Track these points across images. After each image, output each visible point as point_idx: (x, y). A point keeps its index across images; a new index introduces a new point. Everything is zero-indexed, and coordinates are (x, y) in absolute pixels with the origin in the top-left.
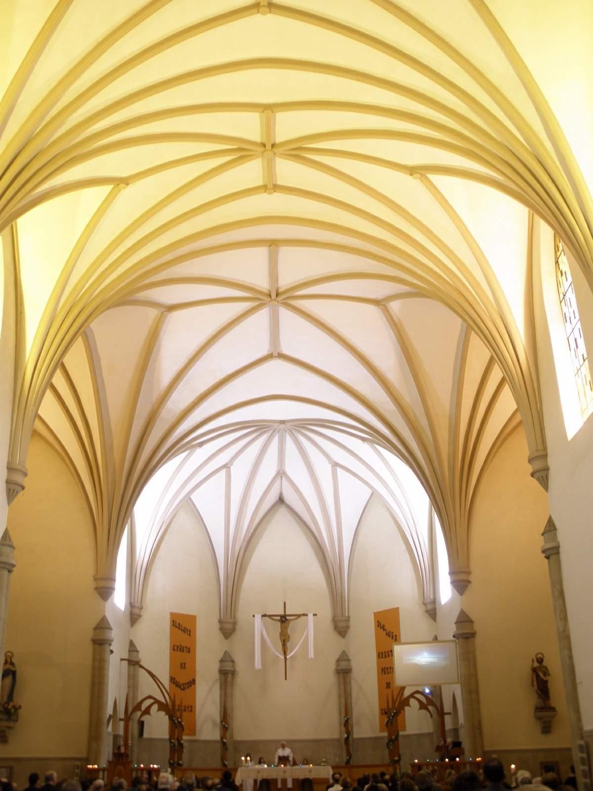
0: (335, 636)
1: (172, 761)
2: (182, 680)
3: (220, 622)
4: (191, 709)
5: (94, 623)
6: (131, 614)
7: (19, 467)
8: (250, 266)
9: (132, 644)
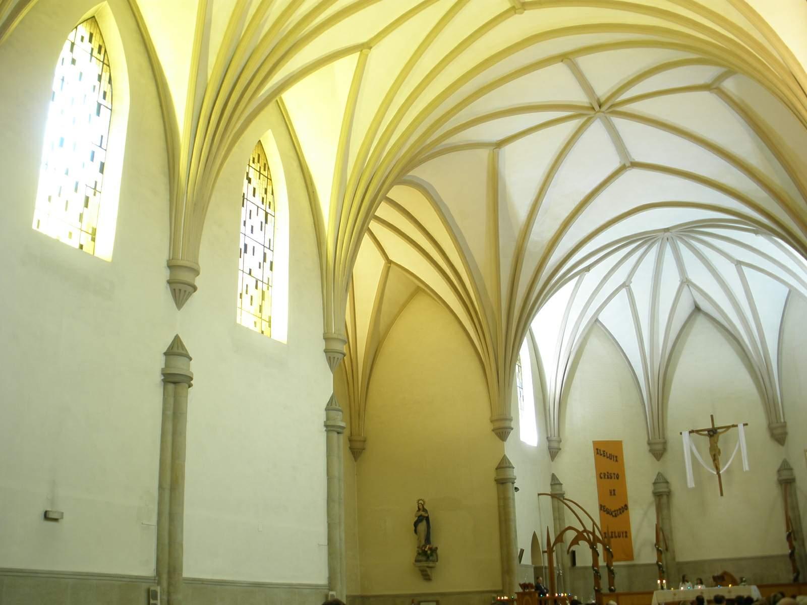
0: (772, 445)
1: (596, 588)
2: (613, 506)
3: (649, 444)
4: (626, 534)
5: (495, 464)
6: (550, 448)
7: (335, 336)
8: (557, 84)
9: (554, 477)
